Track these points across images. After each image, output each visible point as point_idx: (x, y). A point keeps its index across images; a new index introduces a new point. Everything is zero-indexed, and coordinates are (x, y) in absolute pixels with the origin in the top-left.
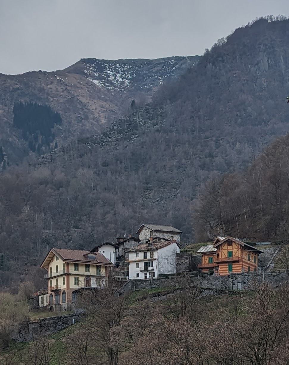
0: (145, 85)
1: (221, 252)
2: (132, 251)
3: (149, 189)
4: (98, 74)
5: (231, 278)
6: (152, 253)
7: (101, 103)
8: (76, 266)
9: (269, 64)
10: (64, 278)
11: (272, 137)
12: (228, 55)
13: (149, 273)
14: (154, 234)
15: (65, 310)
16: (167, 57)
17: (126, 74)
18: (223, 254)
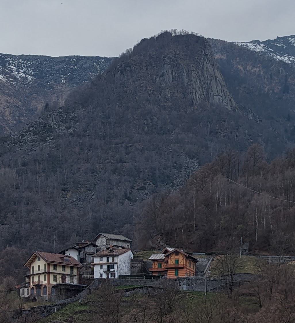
0: (48, 82)
1: (170, 260)
2: (97, 256)
3: (66, 190)
4: (2, 69)
5: (178, 281)
6: (114, 258)
7: (6, 98)
8: (55, 266)
9: (172, 76)
10: (45, 276)
11: (176, 146)
12: (135, 65)
13: (111, 274)
14: (110, 242)
15: (46, 301)
16: (69, 56)
17: (29, 70)
18: (172, 262)
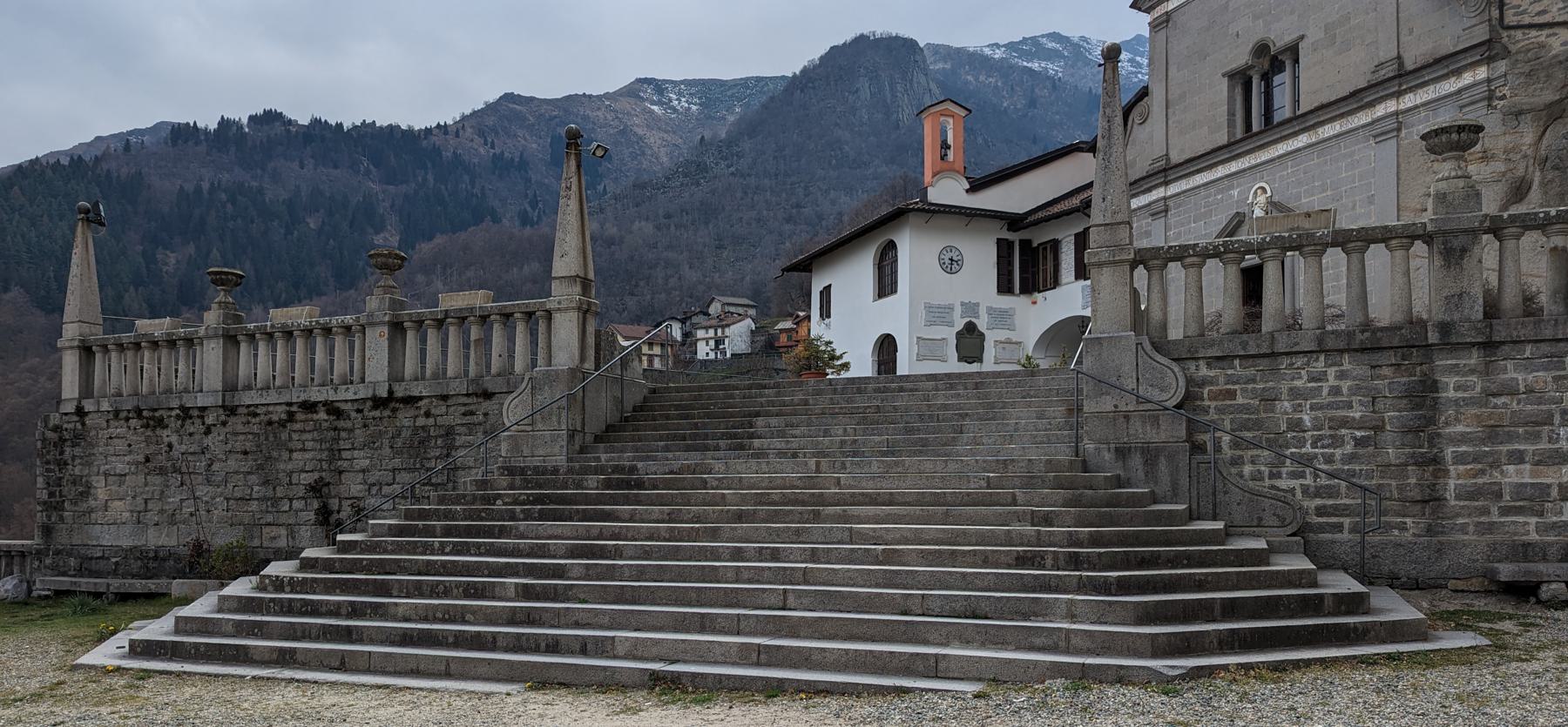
0: (717, 112)
12: (821, 80)
